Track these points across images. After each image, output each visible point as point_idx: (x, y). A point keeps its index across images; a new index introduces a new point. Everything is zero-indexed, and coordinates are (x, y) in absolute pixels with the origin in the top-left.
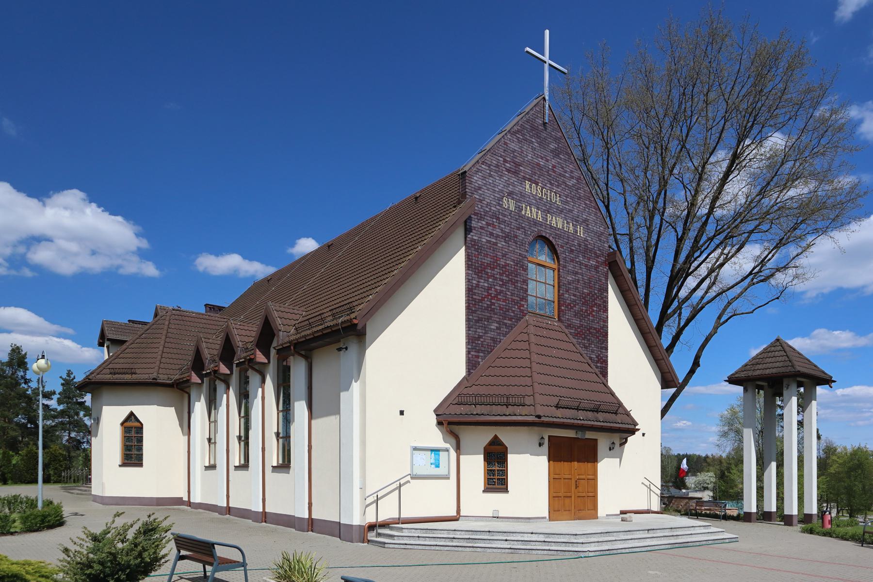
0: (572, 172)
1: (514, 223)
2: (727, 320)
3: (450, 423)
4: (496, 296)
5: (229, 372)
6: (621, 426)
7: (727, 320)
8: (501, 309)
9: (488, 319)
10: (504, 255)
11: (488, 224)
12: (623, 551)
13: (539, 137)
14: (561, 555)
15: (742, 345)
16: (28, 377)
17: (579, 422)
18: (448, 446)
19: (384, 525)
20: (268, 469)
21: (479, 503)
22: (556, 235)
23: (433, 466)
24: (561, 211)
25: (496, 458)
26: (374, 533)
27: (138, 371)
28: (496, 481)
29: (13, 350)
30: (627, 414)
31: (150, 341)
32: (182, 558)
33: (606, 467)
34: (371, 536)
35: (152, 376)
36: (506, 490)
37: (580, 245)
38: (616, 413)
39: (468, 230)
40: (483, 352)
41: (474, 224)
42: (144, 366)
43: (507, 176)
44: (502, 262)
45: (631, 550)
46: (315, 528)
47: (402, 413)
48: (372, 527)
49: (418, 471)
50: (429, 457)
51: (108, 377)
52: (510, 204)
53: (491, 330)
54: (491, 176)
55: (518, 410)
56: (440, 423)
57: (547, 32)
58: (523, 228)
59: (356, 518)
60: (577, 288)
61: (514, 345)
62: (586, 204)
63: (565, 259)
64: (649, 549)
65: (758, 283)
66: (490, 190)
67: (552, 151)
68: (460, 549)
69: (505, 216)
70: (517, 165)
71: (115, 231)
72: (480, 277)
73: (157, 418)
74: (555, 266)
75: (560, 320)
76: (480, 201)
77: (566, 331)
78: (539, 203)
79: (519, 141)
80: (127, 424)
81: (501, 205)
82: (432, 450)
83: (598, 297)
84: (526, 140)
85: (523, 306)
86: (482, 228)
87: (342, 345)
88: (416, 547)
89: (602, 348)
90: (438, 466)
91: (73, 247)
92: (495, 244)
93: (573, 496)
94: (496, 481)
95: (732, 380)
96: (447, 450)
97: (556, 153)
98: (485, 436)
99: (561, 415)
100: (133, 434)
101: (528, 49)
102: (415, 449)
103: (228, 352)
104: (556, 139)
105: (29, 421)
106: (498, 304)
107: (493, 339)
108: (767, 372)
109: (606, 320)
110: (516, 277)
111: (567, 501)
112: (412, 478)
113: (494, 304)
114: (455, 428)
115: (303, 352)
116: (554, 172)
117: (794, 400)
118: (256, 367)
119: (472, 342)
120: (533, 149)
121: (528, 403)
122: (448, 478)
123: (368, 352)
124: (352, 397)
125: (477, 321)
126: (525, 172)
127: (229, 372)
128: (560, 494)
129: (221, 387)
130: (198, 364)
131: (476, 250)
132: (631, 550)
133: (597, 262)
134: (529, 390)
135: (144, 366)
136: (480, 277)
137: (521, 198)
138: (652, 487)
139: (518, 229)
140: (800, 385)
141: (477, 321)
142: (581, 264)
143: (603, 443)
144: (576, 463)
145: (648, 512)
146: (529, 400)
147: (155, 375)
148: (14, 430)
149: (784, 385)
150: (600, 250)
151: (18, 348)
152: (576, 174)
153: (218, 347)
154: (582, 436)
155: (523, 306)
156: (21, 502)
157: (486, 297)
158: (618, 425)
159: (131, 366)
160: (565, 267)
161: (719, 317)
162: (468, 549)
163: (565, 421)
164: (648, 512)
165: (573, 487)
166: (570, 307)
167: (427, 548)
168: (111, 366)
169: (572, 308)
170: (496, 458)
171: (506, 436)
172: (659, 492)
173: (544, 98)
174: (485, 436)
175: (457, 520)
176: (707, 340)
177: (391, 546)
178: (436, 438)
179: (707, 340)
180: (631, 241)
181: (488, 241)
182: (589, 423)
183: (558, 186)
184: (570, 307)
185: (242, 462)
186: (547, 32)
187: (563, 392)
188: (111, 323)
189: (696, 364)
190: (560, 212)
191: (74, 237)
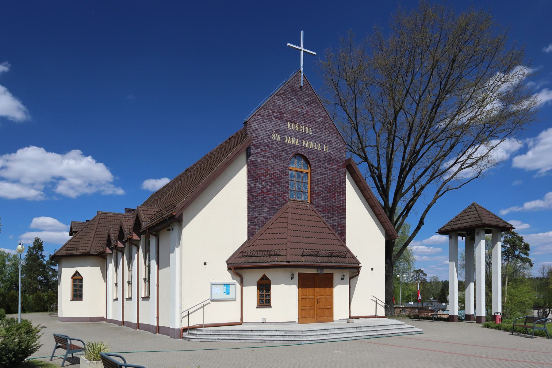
0: (320, 113)
1: (280, 148)
2: (442, 194)
3: (235, 268)
4: (267, 192)
5: (123, 246)
6: (348, 265)
7: (442, 194)
8: (270, 199)
9: (262, 206)
10: (272, 168)
11: (262, 151)
12: (333, 340)
13: (296, 95)
14: (291, 343)
15: (448, 211)
16: (43, 254)
17: (317, 264)
18: (235, 281)
19: (193, 328)
20: (140, 299)
21: (254, 314)
22: (309, 152)
24: (313, 138)
25: (264, 287)
26: (187, 333)
27: (80, 248)
28: (265, 301)
29: (36, 240)
30: (354, 258)
31: (88, 231)
32: (58, 347)
33: (340, 291)
34: (185, 335)
35: (87, 251)
36: (270, 306)
37: (325, 157)
38: (345, 257)
39: (248, 155)
40: (258, 225)
41: (252, 151)
42: (84, 245)
43: (275, 121)
44: (271, 172)
45: (339, 340)
46: (160, 331)
47: (205, 264)
48: (185, 330)
49: (215, 297)
50: (223, 289)
51: (64, 253)
52: (277, 137)
53: (264, 212)
54: (263, 122)
55: (276, 259)
56: (229, 269)
57: (302, 32)
58: (285, 150)
59: (178, 325)
60: (323, 183)
61: (278, 221)
62: (330, 132)
63: (315, 166)
64: (353, 338)
65: (465, 168)
66: (264, 129)
67: (306, 103)
68: (232, 341)
69: (273, 144)
70: (282, 113)
71: (99, 171)
72: (256, 182)
73: (90, 273)
74: (309, 171)
75: (311, 203)
76: (257, 137)
77: (315, 209)
78: (296, 135)
79: (283, 99)
80: (74, 278)
81: (271, 139)
82: (224, 285)
83: (338, 187)
84: (288, 98)
85: (286, 196)
86: (258, 153)
87: (171, 228)
88: (207, 340)
89: (341, 218)
90: (228, 294)
91: (77, 182)
92: (267, 162)
93: (316, 308)
94: (265, 301)
95: (441, 232)
96: (234, 284)
97: (309, 103)
98: (257, 275)
99: (304, 260)
100: (78, 283)
101: (289, 44)
102: (213, 284)
103: (121, 235)
104: (309, 95)
105: (45, 279)
106: (268, 197)
107: (266, 218)
108: (464, 225)
109: (344, 201)
110: (280, 179)
111: (311, 311)
112: (211, 301)
113: (266, 197)
114: (239, 271)
115: (154, 233)
116: (308, 115)
117: (483, 242)
118: (134, 243)
119: (251, 220)
120: (293, 103)
121: (293, 253)
122: (235, 300)
123: (184, 230)
124: (176, 256)
125: (254, 208)
126: (287, 117)
127: (123, 246)
128: (306, 308)
129: (120, 254)
130: (109, 243)
131: (254, 166)
132: (339, 340)
133: (338, 166)
134: (284, 247)
135: (84, 245)
136: (256, 182)
137: (284, 133)
138: (378, 301)
139: (283, 151)
140: (487, 232)
141: (254, 208)
142: (326, 168)
143: (337, 276)
144: (317, 288)
145: (375, 317)
146: (282, 253)
147: (88, 250)
148: (36, 284)
149: (476, 232)
150: (340, 158)
151: (38, 239)
152: (323, 114)
153: (117, 232)
154: (323, 271)
155: (286, 196)
156: (14, 322)
157: (260, 193)
158: (346, 265)
159: (77, 246)
160: (315, 171)
161: (438, 192)
162: (236, 341)
163: (307, 263)
164: (375, 317)
165: (316, 303)
166: (318, 195)
167: (214, 340)
168: (66, 246)
169: (320, 195)
170: (264, 287)
171: (271, 274)
172: (383, 305)
173: (300, 72)
174: (257, 275)
175: (241, 324)
176: (429, 207)
177: (194, 340)
178: (228, 277)
179: (429, 207)
180: (378, 150)
181: (262, 161)
182: (325, 264)
183: (310, 123)
184: (318, 195)
185: (147, 295)
186: (302, 32)
187: (308, 246)
188: (76, 222)
189: (421, 223)
190: (312, 138)
191: (78, 175)
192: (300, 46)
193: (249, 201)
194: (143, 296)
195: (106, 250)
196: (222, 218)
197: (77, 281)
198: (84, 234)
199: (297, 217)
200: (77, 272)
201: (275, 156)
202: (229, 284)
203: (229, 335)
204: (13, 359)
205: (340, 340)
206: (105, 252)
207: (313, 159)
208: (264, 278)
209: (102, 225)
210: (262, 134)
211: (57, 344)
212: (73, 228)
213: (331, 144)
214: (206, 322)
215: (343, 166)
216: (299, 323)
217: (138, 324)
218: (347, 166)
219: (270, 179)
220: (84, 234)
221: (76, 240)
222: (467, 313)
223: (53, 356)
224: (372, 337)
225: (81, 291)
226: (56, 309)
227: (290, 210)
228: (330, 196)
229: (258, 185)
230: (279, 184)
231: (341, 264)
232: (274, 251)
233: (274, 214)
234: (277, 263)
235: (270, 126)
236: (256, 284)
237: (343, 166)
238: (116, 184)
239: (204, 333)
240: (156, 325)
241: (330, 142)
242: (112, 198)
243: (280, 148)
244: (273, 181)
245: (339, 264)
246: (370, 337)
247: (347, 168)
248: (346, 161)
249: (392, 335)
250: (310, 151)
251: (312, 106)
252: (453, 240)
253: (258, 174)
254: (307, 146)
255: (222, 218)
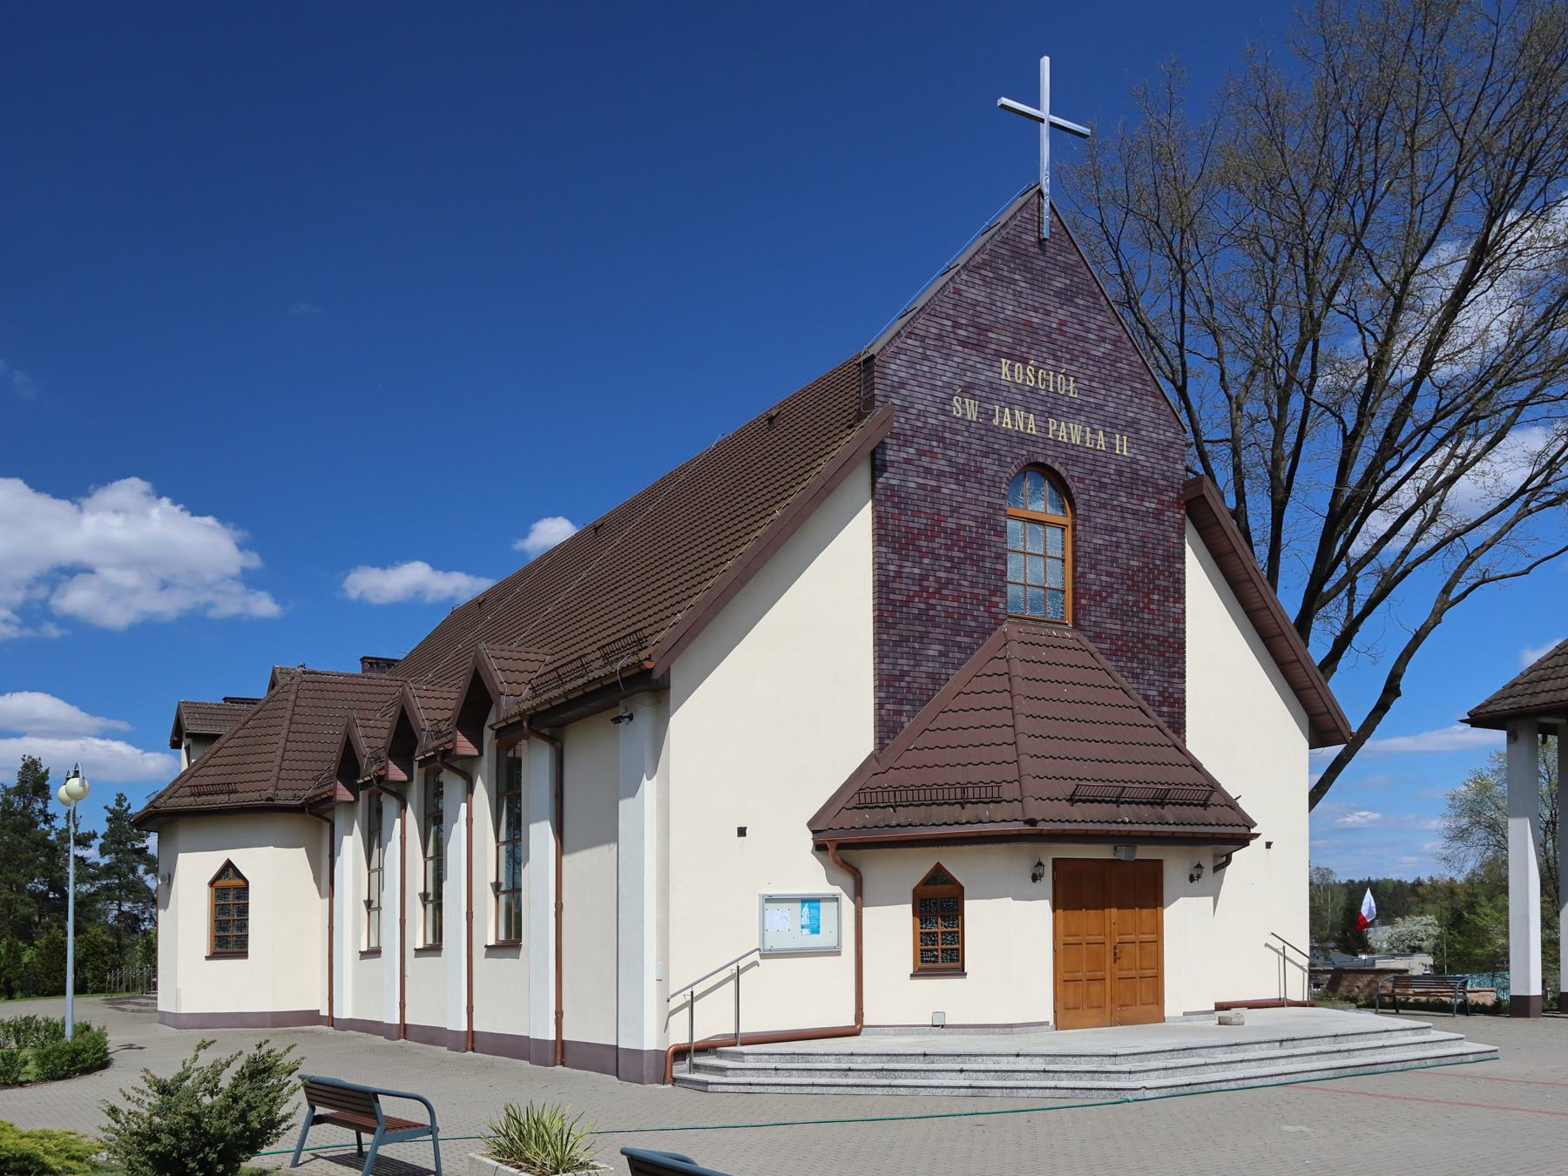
0: (1101, 329)
1: (976, 446)
2: (1465, 595)
3: (841, 846)
7: (1465, 595)
8: (948, 615)
9: (922, 637)
10: (954, 510)
11: (921, 453)
13: (1028, 270)
14: (1082, 1099)
16: (50, 811)
17: (1121, 827)
18: (837, 890)
19: (706, 1048)
21: (902, 999)
22: (1068, 457)
23: (806, 931)
24: (1080, 410)
25: (939, 910)
27: (240, 787)
28: (940, 953)
29: (26, 766)
30: (1232, 805)
32: (318, 1120)
34: (680, 1070)
35: (265, 795)
37: (1120, 473)
38: (1205, 805)
39: (878, 467)
40: (909, 702)
41: (891, 455)
44: (951, 524)
46: (568, 1059)
47: (742, 832)
48: (681, 1053)
49: (774, 943)
51: (188, 802)
54: (925, 357)
55: (986, 811)
56: (819, 848)
57: (1046, 62)
59: (651, 1041)
60: (1114, 560)
61: (977, 685)
62: (1133, 389)
63: (1087, 504)
64: (1283, 1079)
65: (1539, 508)
66: (923, 387)
67: (1058, 294)
68: (863, 1091)
69: (955, 432)
70: (982, 330)
71: (199, 543)
73: (274, 870)
74: (1067, 520)
76: (904, 409)
77: (1092, 647)
78: (1029, 399)
80: (220, 883)
83: (1161, 573)
84: (1000, 278)
85: (996, 605)
86: (907, 461)
87: (621, 712)
89: (1172, 675)
91: (129, 578)
92: (937, 489)
93: (1109, 974)
94: (940, 953)
95: (1479, 719)
96: (836, 899)
97: (1066, 296)
98: (915, 868)
100: (231, 900)
101: (1005, 101)
102: (770, 899)
103: (403, 742)
104: (1067, 269)
105: (52, 888)
107: (931, 676)
109: (1180, 619)
110: (982, 550)
111: (1095, 988)
112: (763, 956)
113: (933, 607)
114: (853, 855)
115: (546, 731)
116: (1063, 333)
122: (838, 953)
124: (643, 809)
125: (897, 644)
128: (1080, 975)
130: (348, 767)
133: (1160, 502)
134: (1010, 772)
138: (1290, 952)
139: (986, 455)
141: (897, 644)
142: (1124, 510)
143: (1175, 868)
144: (1114, 911)
150: (1165, 478)
153: (385, 733)
155: (996, 605)
159: (229, 779)
160: (1088, 519)
161: (1447, 590)
163: (1090, 826)
165: (1109, 959)
166: (1098, 598)
168: (193, 782)
169: (1104, 600)
170: (939, 910)
171: (959, 864)
172: (1305, 962)
173: (1040, 193)
174: (915, 868)
175: (857, 1034)
176: (1418, 638)
177: (720, 1088)
178: (813, 876)
179: (1418, 638)
180: (1236, 452)
181: (921, 486)
182: (1144, 827)
183: (1071, 361)
184: (1098, 598)
185: (430, 941)
186: (1046, 62)
187: (1085, 770)
188: (194, 705)
189: (1392, 690)
192: (1037, 106)
193: (883, 621)
194: (420, 945)
195: (334, 790)
196: (792, 684)
197: (230, 896)
198: (249, 741)
199: (1039, 671)
200: (229, 865)
201: (962, 472)
202: (818, 900)
203: (827, 1070)
204: (221, 1167)
205: (1288, 1082)
206: (330, 798)
207: (1081, 480)
208: (938, 876)
209: (307, 711)
210: (922, 400)
211: (313, 1109)
212: (185, 722)
213: (1137, 431)
214: (745, 1029)
215: (1176, 504)
216: (1058, 1025)
217: (471, 1034)
218: (1187, 503)
219: (948, 548)
220: (249, 741)
221: (224, 760)
222: (1516, 990)
223: (300, 1149)
224: (1342, 1073)
225: (244, 925)
226: (152, 986)
227: (1015, 650)
228: (1136, 603)
229: (911, 569)
230: (977, 562)
231: (1195, 829)
232: (907, 788)
233: (961, 662)
234: (990, 827)
235: (946, 372)
236: (910, 896)
237: (1176, 504)
238: (250, 580)
239: (750, 1063)
240: (552, 1037)
241: (1133, 424)
242: (241, 626)
243: (976, 446)
244: (956, 554)
245: (1188, 829)
246: (1338, 1073)
247: (1188, 512)
248: (1187, 485)
249: (1404, 1067)
250: (1073, 454)
251: (1077, 306)
252: (1523, 746)
253: (909, 530)
254: (1062, 436)
255: (792, 684)
